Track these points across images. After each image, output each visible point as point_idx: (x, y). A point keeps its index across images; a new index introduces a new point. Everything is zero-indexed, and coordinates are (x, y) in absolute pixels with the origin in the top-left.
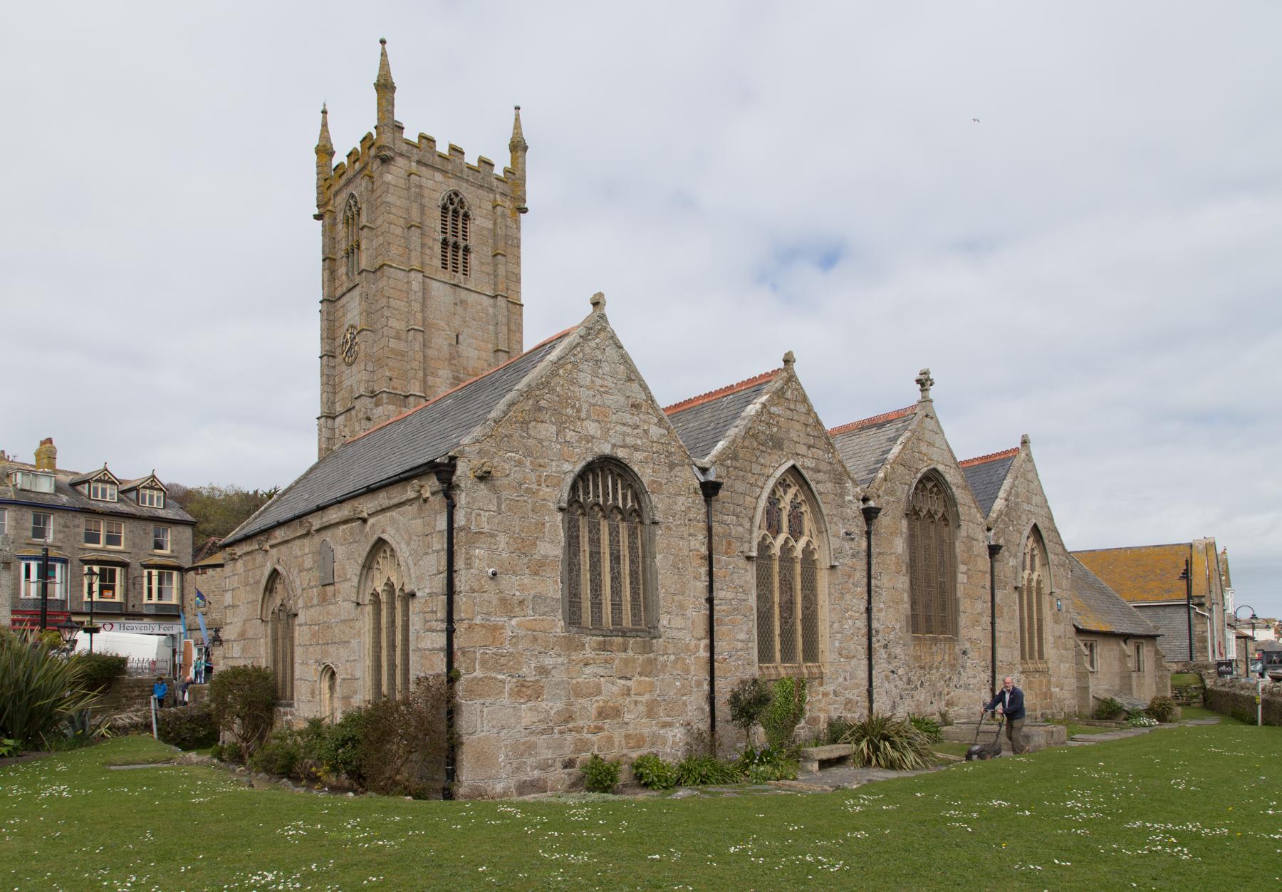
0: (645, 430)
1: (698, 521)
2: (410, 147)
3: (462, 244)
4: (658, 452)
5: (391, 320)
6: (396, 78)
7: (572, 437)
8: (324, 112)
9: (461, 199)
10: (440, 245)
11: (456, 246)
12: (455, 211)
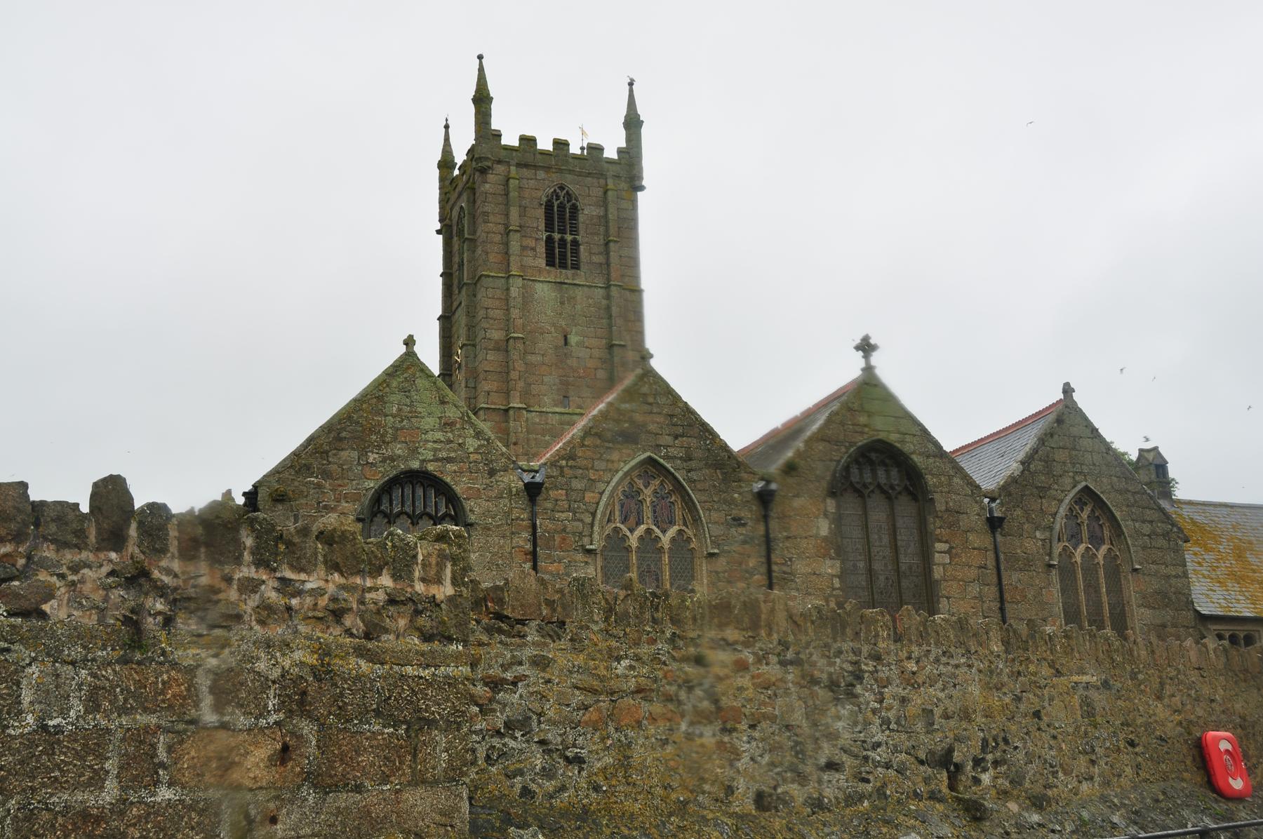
0: (460, 444)
1: (522, 520)
2: (509, 152)
3: (569, 238)
4: (475, 462)
6: (493, 89)
7: (375, 459)
8: (447, 127)
9: (567, 192)
10: (543, 244)
11: (563, 242)
12: (562, 207)
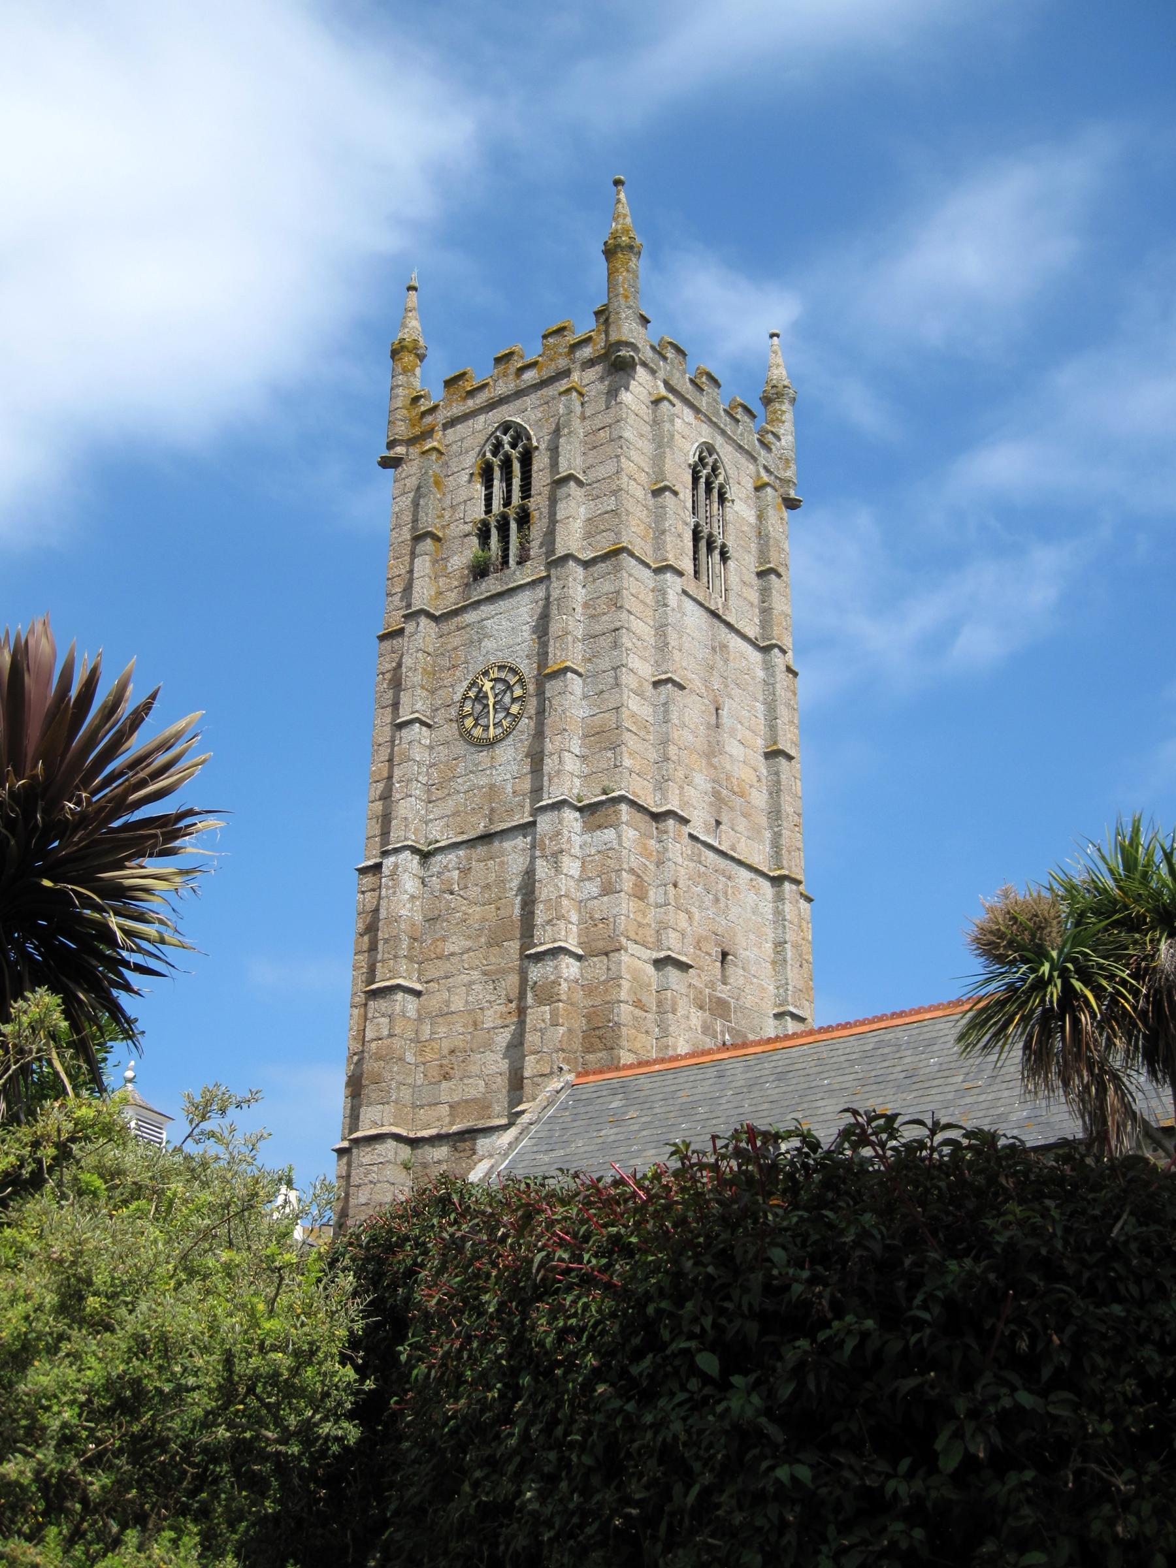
5: (631, 655)
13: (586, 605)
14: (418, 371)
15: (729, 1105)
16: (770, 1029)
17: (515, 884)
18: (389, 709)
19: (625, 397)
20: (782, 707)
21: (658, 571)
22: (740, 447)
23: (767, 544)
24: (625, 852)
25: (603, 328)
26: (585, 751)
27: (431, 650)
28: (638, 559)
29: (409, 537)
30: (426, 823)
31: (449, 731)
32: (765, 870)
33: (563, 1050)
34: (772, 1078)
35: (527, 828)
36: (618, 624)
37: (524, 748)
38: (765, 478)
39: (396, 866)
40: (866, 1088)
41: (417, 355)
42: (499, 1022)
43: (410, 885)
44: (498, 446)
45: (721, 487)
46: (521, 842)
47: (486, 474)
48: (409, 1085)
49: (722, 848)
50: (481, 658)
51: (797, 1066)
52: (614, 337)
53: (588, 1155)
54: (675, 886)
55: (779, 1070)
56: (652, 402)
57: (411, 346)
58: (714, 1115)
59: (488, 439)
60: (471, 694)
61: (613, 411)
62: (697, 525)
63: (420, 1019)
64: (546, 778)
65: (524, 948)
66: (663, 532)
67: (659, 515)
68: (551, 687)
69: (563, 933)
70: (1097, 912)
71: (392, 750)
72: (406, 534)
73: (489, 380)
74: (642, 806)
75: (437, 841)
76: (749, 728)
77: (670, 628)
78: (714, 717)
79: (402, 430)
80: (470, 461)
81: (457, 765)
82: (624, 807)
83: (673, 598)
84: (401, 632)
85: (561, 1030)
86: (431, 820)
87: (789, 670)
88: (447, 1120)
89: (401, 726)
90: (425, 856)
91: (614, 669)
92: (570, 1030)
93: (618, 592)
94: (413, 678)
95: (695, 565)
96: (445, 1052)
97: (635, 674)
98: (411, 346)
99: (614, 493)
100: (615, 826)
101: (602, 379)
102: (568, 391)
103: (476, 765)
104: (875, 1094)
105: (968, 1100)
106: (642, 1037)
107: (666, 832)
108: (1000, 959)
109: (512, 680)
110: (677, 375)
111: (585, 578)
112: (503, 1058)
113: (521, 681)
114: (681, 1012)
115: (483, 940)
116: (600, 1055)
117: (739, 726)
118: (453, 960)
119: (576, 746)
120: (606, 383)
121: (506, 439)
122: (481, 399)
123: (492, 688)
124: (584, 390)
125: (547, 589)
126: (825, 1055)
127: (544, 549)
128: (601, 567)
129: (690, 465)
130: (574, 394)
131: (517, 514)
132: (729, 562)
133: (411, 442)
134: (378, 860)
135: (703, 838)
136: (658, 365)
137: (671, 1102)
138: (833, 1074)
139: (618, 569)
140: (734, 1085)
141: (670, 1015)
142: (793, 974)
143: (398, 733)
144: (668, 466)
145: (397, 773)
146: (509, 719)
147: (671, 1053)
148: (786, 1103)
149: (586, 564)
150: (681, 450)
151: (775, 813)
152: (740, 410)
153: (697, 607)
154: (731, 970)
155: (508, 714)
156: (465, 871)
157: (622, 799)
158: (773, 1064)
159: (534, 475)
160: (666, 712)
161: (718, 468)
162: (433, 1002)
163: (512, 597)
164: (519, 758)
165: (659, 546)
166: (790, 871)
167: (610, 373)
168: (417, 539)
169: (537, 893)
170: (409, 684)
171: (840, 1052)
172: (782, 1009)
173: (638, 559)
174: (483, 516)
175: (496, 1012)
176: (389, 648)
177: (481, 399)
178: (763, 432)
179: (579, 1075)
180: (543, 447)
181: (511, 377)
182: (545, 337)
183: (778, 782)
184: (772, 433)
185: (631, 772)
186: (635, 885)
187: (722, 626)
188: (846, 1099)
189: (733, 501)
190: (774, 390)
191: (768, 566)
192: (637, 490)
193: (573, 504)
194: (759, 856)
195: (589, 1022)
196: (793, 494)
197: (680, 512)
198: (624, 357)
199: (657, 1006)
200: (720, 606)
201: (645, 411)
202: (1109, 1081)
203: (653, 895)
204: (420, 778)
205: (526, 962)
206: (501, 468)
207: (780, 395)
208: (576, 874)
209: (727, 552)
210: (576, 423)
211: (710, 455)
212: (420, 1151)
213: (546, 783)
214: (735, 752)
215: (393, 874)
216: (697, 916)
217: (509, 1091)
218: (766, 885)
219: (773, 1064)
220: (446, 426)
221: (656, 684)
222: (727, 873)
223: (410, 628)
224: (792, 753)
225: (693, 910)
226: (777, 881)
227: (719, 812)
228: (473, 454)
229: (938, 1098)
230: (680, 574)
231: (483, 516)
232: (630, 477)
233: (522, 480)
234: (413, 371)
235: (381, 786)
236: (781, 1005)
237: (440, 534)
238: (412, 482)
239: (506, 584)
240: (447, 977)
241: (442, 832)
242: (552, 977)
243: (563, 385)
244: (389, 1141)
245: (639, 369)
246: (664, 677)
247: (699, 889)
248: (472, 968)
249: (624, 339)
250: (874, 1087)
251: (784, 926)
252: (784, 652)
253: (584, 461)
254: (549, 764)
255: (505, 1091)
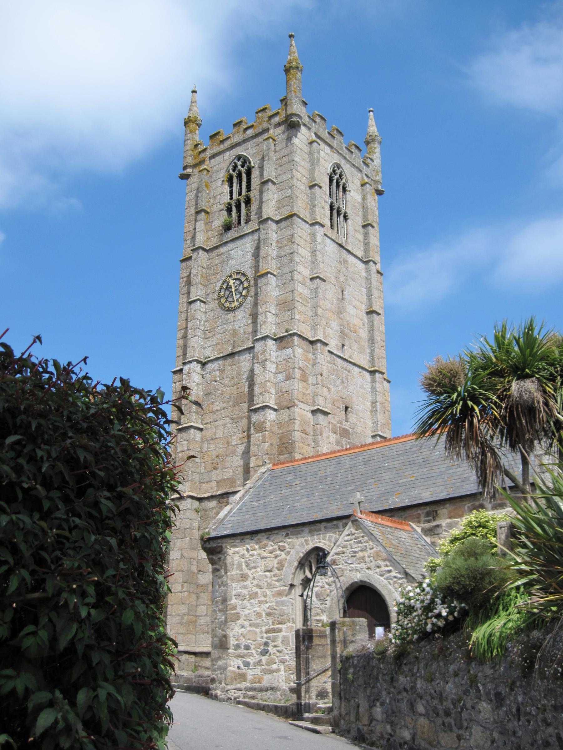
13: (277, 242)
14: (197, 132)
15: (342, 477)
16: (370, 440)
17: (245, 376)
18: (186, 295)
19: (295, 141)
20: (375, 290)
21: (312, 225)
22: (354, 165)
23: (367, 211)
24: (296, 360)
25: (284, 107)
26: (278, 312)
27: (205, 266)
28: (302, 219)
29: (194, 212)
30: (204, 349)
31: (214, 304)
32: (367, 368)
33: (268, 454)
34: (362, 463)
35: (250, 349)
36: (292, 251)
37: (249, 312)
38: (366, 180)
39: (190, 369)
40: (405, 467)
41: (197, 124)
42: (239, 442)
43: (196, 378)
44: (235, 167)
45: (344, 184)
46: (248, 356)
47: (230, 180)
48: (198, 473)
49: (345, 357)
50: (228, 269)
51: (374, 458)
52: (289, 112)
53: (275, 502)
54: (321, 375)
55: (366, 460)
56: (309, 143)
57: (193, 120)
58: (334, 482)
59: (230, 164)
60: (224, 286)
61: (289, 148)
62: (332, 203)
63: (202, 442)
64: (259, 325)
65: (250, 406)
66: (314, 206)
67: (313, 198)
68: (261, 282)
69: (268, 399)
70: (482, 368)
71: (187, 314)
72: (193, 211)
73: (231, 135)
74: (304, 338)
75: (209, 357)
76: (359, 300)
77: (318, 252)
78: (341, 295)
79: (190, 161)
80: (222, 175)
81: (218, 321)
82: (296, 338)
83: (319, 238)
84: (190, 258)
85: (267, 444)
86: (206, 347)
87: (378, 272)
88: (215, 489)
89: (191, 303)
90: (203, 364)
91: (291, 272)
92: (271, 445)
93: (292, 235)
94: (196, 280)
95: (331, 222)
96: (214, 457)
97: (301, 274)
98: (193, 120)
99: (291, 187)
100: (292, 347)
101: (284, 132)
102: (268, 139)
103: (227, 320)
104: (409, 469)
105: (452, 471)
106: (306, 447)
107: (317, 350)
108: (433, 392)
109: (243, 279)
110: (321, 130)
111: (277, 229)
112: (241, 459)
113: (247, 279)
114: (325, 435)
115: (231, 403)
116: (286, 456)
117: (354, 299)
118: (218, 413)
119: (273, 310)
120: (286, 134)
121: (239, 163)
122: (227, 144)
123: (234, 283)
124: (276, 138)
125: (259, 235)
126: (387, 452)
127: (257, 216)
128: (284, 223)
129: (328, 174)
130: (271, 140)
131: (245, 199)
132: (348, 221)
133: (195, 166)
134: (181, 367)
135: (335, 352)
136: (312, 125)
137: (315, 476)
138: (390, 461)
139: (292, 224)
140: (344, 467)
141: (319, 437)
142: (380, 417)
143: (189, 307)
144: (317, 174)
145: (190, 325)
146: (242, 298)
147: (320, 453)
148: (367, 475)
149: (277, 222)
150: (324, 167)
151: (372, 341)
152: (353, 147)
153: (332, 242)
154: (350, 415)
155: (241, 295)
156: (222, 371)
157: (295, 334)
158: (363, 457)
159: (252, 180)
160: (316, 292)
161: (342, 175)
162: (208, 434)
163: (242, 239)
164: (247, 316)
165: (312, 212)
166: (379, 368)
167: (288, 129)
168: (198, 213)
169: (255, 380)
170: (195, 283)
171: (394, 451)
172: (375, 433)
173: (302, 219)
174: (229, 201)
175: (237, 437)
176: (185, 266)
177: (227, 144)
178: (365, 158)
179: (274, 465)
180: (256, 166)
181: (241, 133)
182: (257, 113)
183: (373, 326)
184: (370, 158)
185: (299, 321)
186: (302, 375)
187: (345, 251)
188: (395, 472)
189: (350, 191)
190: (371, 138)
191: (368, 222)
192: (301, 186)
193: (270, 193)
194: (364, 361)
195: (280, 440)
196: (380, 188)
197: (323, 196)
198: (294, 121)
199: (314, 433)
200: (344, 242)
201: (305, 148)
202: (488, 451)
203: (311, 380)
204: (201, 328)
205: (250, 413)
206: (237, 177)
207: (373, 140)
208: (274, 371)
209: (347, 216)
210: (272, 154)
211: (339, 169)
212: (203, 504)
213: (259, 328)
214: (351, 312)
215: (188, 374)
216: (333, 390)
217: (244, 474)
218: (367, 375)
219: (363, 457)
220: (210, 158)
221: (312, 279)
222: (348, 369)
223: (194, 255)
224: (380, 312)
225: (331, 387)
226: (372, 373)
227: (344, 340)
228: (224, 171)
229: (438, 470)
230: (323, 226)
231: (229, 201)
232: (298, 180)
233: (247, 183)
234: (195, 132)
235: (182, 332)
236: (375, 431)
237: (209, 210)
238: (195, 186)
239: (240, 233)
240: (214, 422)
241: (211, 353)
242: (263, 420)
243: (266, 136)
244: (189, 499)
245: (302, 127)
246: (315, 276)
247: (334, 377)
248: (226, 417)
249: (294, 112)
250: (409, 466)
251: (376, 394)
252: (376, 264)
253: (276, 173)
254: (260, 319)
255: (242, 474)
